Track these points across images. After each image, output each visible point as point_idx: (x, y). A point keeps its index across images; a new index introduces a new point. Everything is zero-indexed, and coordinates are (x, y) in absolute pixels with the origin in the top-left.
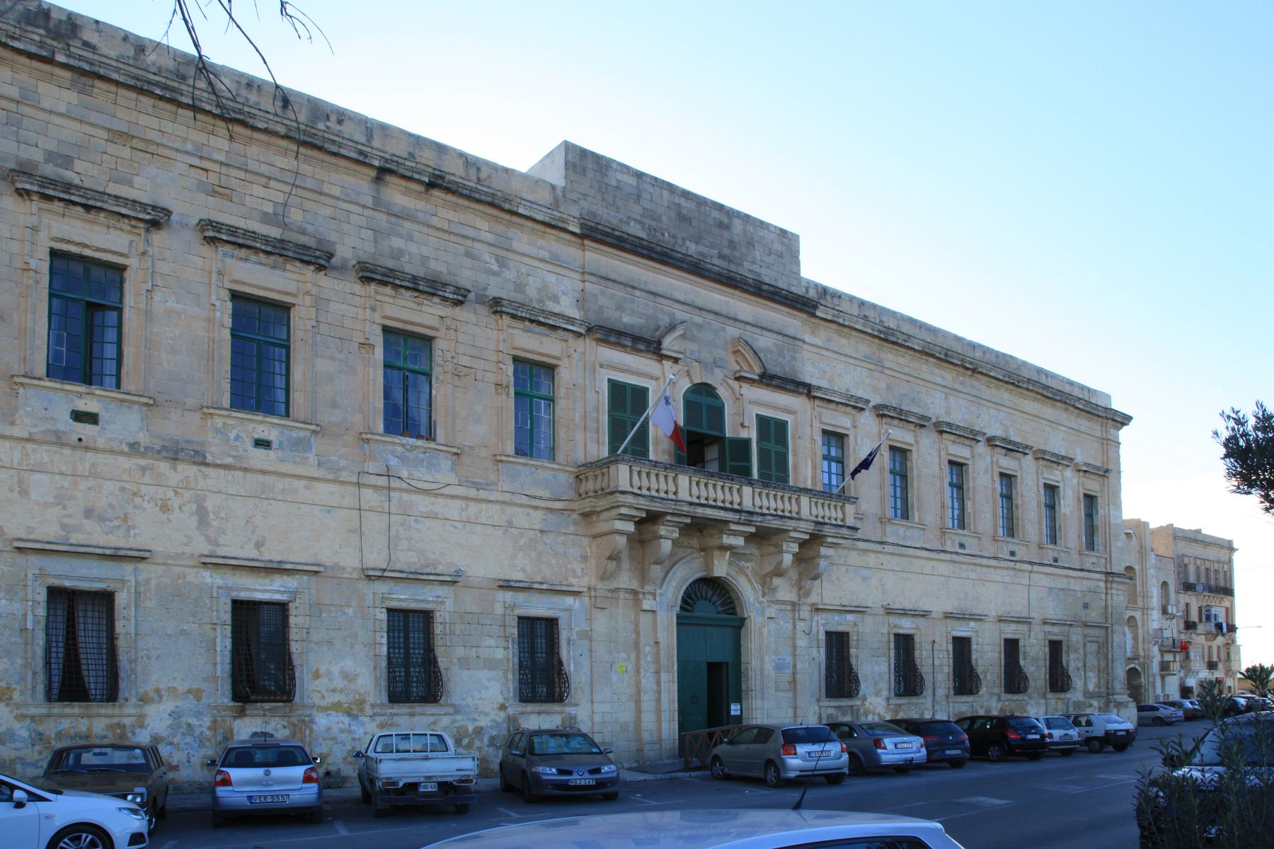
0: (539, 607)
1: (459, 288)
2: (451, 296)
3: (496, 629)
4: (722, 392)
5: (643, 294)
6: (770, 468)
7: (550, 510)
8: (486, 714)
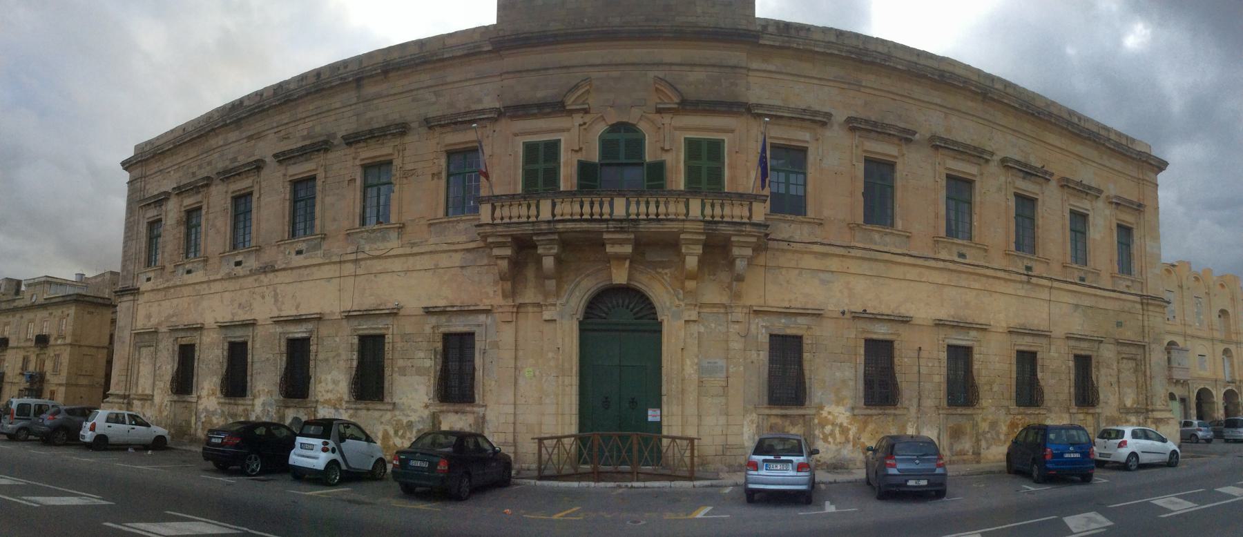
3: (425, 344)
4: (643, 126)
7: (468, 250)
8: (415, 411)
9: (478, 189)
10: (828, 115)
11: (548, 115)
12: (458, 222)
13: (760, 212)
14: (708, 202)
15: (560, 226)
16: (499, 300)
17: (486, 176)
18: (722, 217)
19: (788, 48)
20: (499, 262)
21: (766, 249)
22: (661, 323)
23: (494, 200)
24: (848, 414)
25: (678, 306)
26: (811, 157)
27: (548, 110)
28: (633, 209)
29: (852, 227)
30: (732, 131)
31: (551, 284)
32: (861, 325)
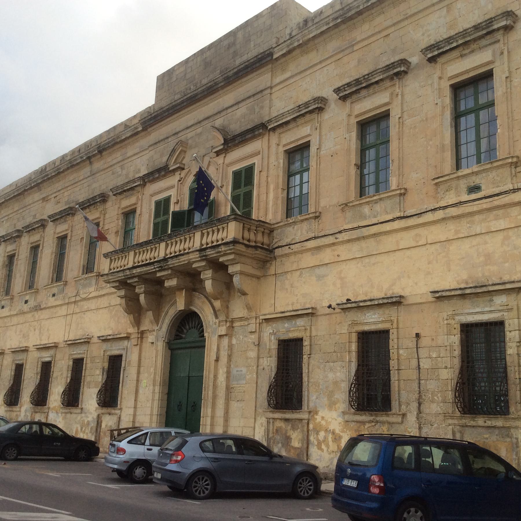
19: (294, 49)
21: (275, 258)
24: (340, 420)
29: (345, 206)
32: (352, 316)
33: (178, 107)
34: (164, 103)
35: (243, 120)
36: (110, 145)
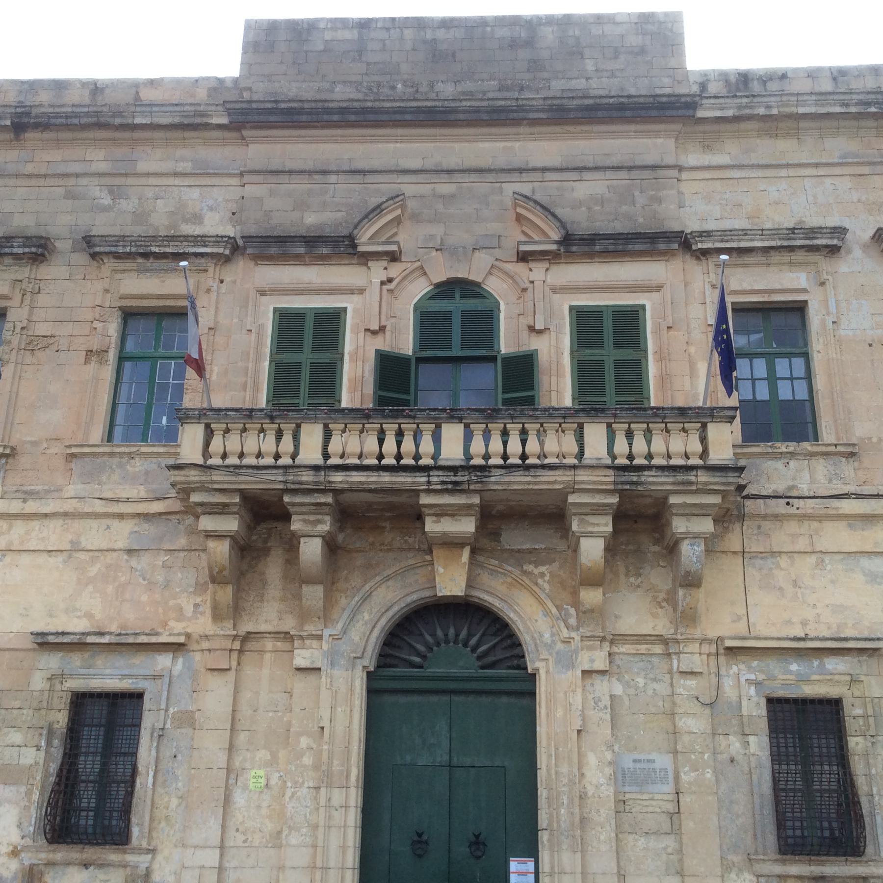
0: (109, 676)
1: (27, 238)
2: (20, 251)
4: (495, 286)
5: (342, 177)
6: (600, 390)
9: (179, 391)
10: (840, 231)
11: (323, 259)
12: (131, 456)
13: (724, 442)
14: (620, 428)
15: (338, 478)
16: (204, 624)
17: (199, 367)
18: (650, 456)
20: (212, 544)
21: (742, 518)
22: (533, 678)
23: (212, 418)
25: (567, 642)
26: (815, 317)
27: (325, 251)
28: (477, 446)
30: (658, 288)
31: (314, 594)
33: (385, 117)
34: (260, 90)
35: (597, 208)
36: (76, 121)
